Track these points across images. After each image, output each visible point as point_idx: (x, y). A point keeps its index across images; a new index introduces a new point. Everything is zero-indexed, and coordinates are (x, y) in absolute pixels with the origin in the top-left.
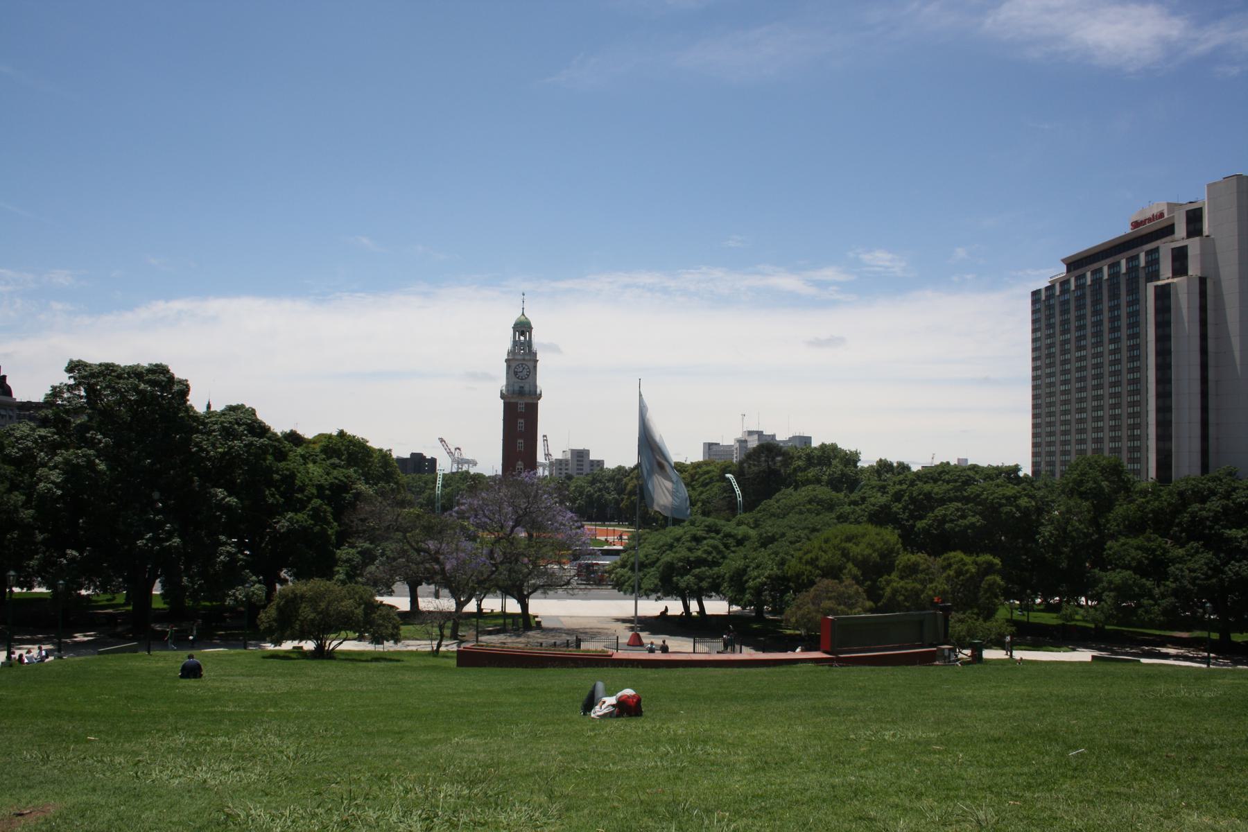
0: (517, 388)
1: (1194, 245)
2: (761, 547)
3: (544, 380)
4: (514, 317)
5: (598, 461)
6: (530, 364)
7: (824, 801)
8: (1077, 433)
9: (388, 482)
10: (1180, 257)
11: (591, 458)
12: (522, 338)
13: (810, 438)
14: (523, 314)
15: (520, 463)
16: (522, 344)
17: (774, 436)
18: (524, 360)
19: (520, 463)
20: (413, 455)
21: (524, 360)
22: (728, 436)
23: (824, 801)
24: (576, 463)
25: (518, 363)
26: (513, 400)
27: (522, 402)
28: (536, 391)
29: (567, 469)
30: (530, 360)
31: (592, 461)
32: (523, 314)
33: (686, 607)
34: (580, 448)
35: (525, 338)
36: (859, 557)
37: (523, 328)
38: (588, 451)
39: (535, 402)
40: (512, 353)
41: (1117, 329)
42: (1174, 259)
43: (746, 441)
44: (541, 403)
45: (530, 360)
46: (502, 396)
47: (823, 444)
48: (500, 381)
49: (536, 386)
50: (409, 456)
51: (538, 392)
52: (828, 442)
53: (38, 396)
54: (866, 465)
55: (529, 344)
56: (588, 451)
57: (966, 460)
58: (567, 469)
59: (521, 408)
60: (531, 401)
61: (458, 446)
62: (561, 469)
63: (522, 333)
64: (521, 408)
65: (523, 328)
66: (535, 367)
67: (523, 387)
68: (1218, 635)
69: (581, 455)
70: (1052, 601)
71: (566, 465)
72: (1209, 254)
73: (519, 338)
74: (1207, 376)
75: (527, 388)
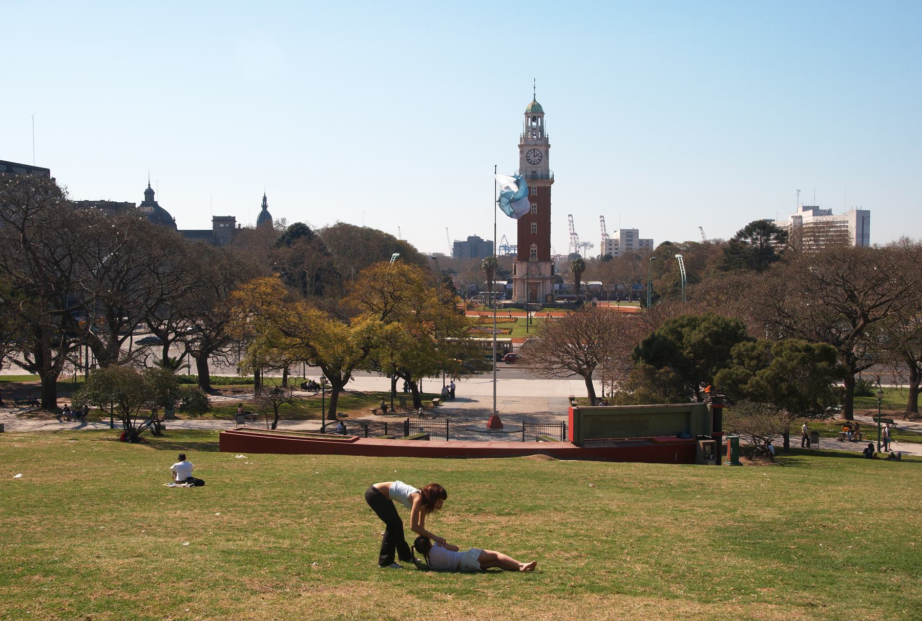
0: (529, 173)
3: (556, 164)
4: (527, 105)
5: (647, 241)
6: (542, 149)
7: (158, 274)
11: (640, 238)
12: (534, 124)
13: (869, 211)
14: (535, 101)
15: (534, 245)
16: (535, 129)
19: (534, 245)
20: (469, 238)
21: (536, 145)
23: (158, 274)
24: (625, 242)
25: (531, 148)
28: (548, 175)
29: (617, 249)
30: (542, 145)
31: (641, 241)
32: (535, 101)
34: (630, 227)
35: (538, 124)
36: (732, 324)
37: (535, 113)
38: (638, 230)
40: (524, 138)
43: (801, 217)
44: (554, 188)
49: (548, 170)
50: (466, 240)
55: (541, 129)
56: (638, 230)
58: (617, 249)
61: (570, 214)
62: (610, 249)
63: (534, 119)
65: (535, 113)
66: (547, 152)
69: (629, 235)
71: (616, 245)
73: (531, 124)
75: (539, 173)
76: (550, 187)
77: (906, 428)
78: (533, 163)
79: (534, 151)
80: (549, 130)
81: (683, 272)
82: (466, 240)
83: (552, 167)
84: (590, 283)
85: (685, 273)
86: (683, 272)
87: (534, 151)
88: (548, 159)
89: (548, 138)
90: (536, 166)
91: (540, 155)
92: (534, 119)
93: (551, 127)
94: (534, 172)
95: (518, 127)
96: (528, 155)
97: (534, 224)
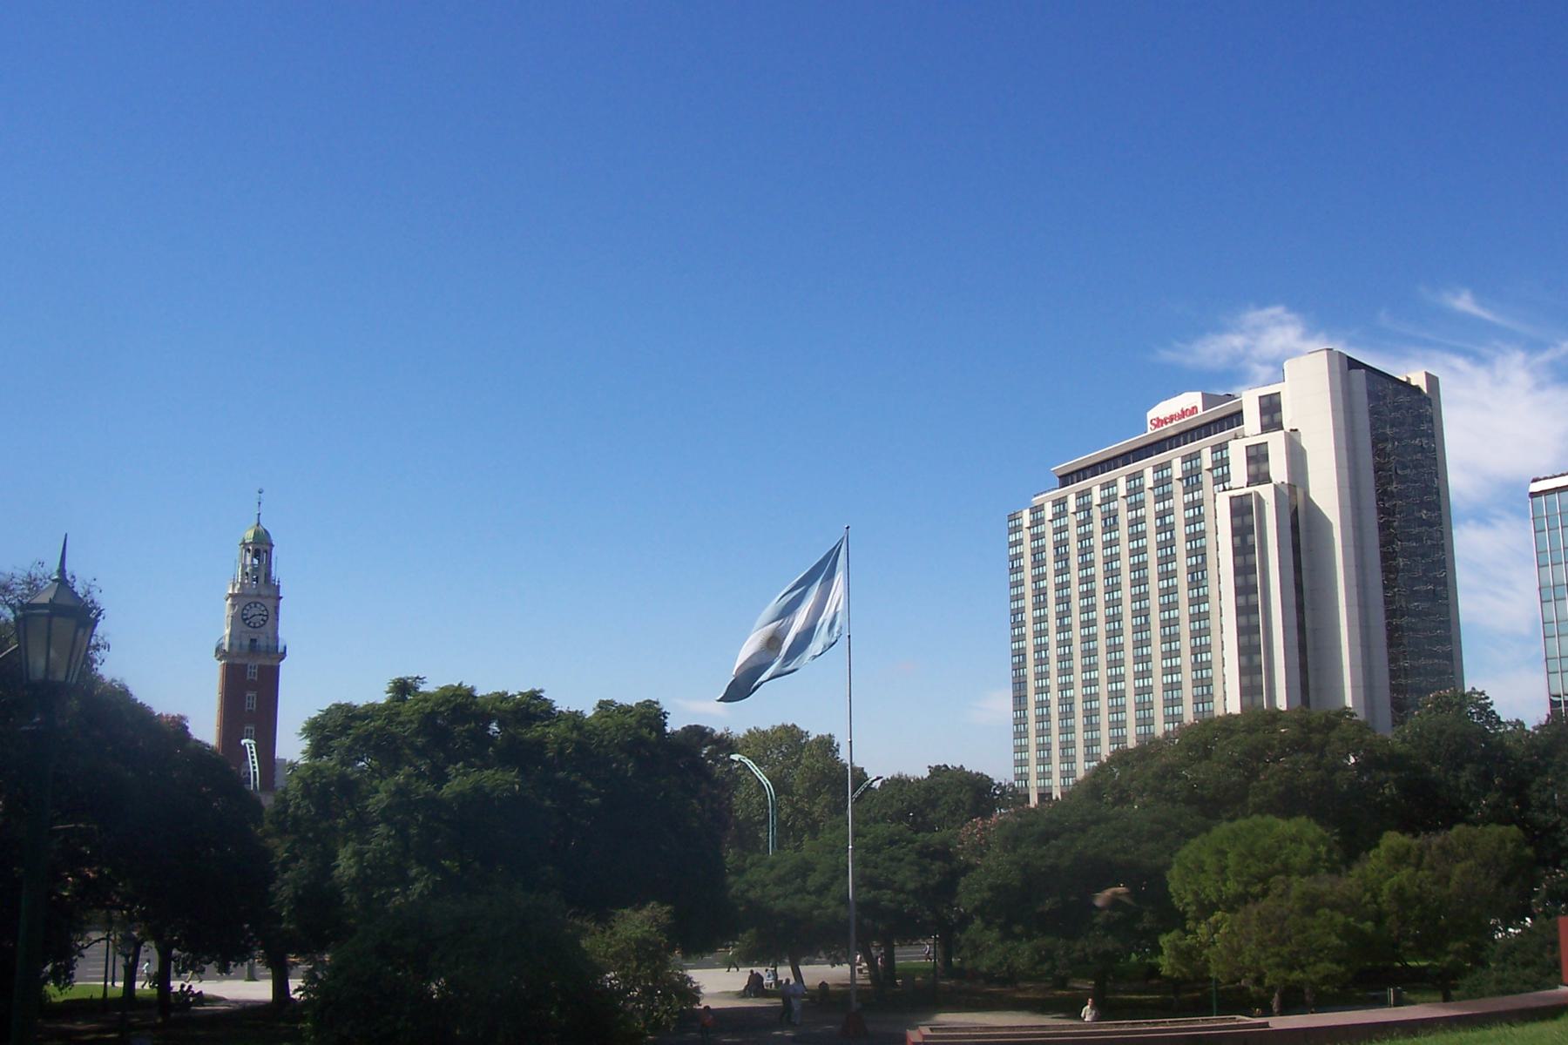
1: (1276, 444)
2: (1417, 871)
3: (290, 629)
6: (269, 604)
8: (1123, 691)
10: (1257, 456)
17: (472, 689)
18: (259, 595)
22: (779, 724)
25: (249, 600)
26: (238, 661)
27: (254, 664)
28: (277, 647)
30: (269, 596)
32: (258, 524)
33: (280, 988)
37: (261, 547)
39: (274, 663)
42: (1250, 459)
44: (284, 666)
45: (269, 596)
46: (220, 652)
47: (535, 695)
48: (221, 627)
49: (276, 639)
51: (281, 649)
52: (693, 724)
53: (928, 774)
54: (678, 728)
57: (507, 693)
59: (252, 675)
60: (267, 662)
64: (252, 675)
65: (261, 547)
66: (277, 608)
67: (255, 640)
68: (780, 1001)
72: (1296, 456)
73: (252, 561)
75: (262, 642)
76: (279, 666)
78: (253, 605)
79: (247, 619)
80: (278, 572)
81: (254, 768)
82: (926, 774)
83: (284, 634)
85: (257, 770)
86: (254, 768)
87: (247, 619)
88: (278, 620)
89: (278, 586)
90: (257, 630)
91: (265, 618)
92: (257, 554)
93: (282, 569)
94: (253, 641)
95: (229, 573)
96: (245, 612)
97: (249, 728)
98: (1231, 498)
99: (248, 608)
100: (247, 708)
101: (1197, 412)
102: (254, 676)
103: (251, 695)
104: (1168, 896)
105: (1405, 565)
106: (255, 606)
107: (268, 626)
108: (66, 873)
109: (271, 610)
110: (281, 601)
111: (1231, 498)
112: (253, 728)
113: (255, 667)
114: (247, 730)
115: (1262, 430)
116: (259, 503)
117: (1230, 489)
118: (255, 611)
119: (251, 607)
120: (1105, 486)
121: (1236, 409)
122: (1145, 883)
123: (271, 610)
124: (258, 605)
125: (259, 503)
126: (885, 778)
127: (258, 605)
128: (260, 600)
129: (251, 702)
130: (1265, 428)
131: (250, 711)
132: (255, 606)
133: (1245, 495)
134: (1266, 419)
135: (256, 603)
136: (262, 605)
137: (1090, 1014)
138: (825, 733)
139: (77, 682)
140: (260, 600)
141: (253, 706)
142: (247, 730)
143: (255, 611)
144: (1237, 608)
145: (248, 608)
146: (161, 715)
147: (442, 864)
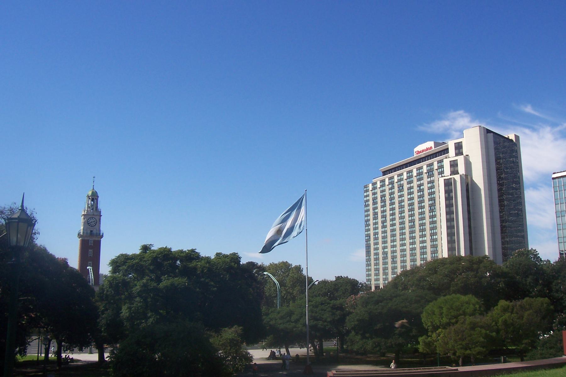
3: (105, 227)
5: (562, 348)
6: (97, 218)
9: (356, 293)
10: (454, 165)
17: (171, 249)
18: (93, 215)
22: (281, 261)
25: (90, 217)
26: (86, 238)
27: (92, 239)
28: (100, 233)
30: (97, 215)
32: (93, 189)
37: (94, 197)
39: (99, 239)
41: (410, 205)
42: (451, 166)
44: (103, 240)
45: (97, 215)
46: (79, 235)
47: (193, 251)
48: (80, 226)
49: (100, 230)
51: (101, 234)
52: (250, 261)
53: (335, 279)
54: (245, 263)
57: (183, 250)
59: (91, 243)
60: (97, 239)
64: (91, 243)
65: (94, 197)
66: (100, 219)
67: (92, 231)
70: (160, 311)
72: (468, 165)
73: (91, 202)
74: (469, 235)
75: (95, 232)
76: (101, 240)
77: (281, 226)
78: (91, 218)
79: (89, 223)
80: (100, 206)
81: (92, 277)
83: (102, 229)
84: (26, 298)
85: (93, 278)
86: (92, 277)
88: (100, 224)
89: (101, 212)
90: (93, 227)
91: (96, 223)
92: (93, 200)
93: (102, 205)
94: (92, 231)
95: (83, 207)
96: (89, 221)
97: (90, 263)
98: (444, 180)
99: (89, 219)
100: (89, 256)
101: (432, 149)
102: (92, 244)
103: (91, 251)
104: (422, 323)
105: (507, 204)
106: (92, 219)
107: (97, 226)
108: (24, 315)
109: (98, 220)
110: (102, 217)
111: (444, 180)
112: (91, 263)
113: (92, 241)
114: (89, 263)
115: (456, 155)
116: (94, 182)
117: (444, 176)
118: (92, 220)
119: (91, 219)
120: (399, 175)
121: (446, 148)
122: (413, 318)
123: (98, 220)
124: (93, 218)
125: (94, 182)
126: (319, 281)
127: (93, 218)
128: (94, 216)
129: (91, 253)
130: (457, 155)
131: (90, 257)
132: (92, 219)
133: (450, 179)
134: (457, 151)
135: (92, 218)
136: (95, 218)
137: (394, 366)
138: (298, 265)
139: (28, 246)
140: (94, 216)
141: (91, 255)
142: (89, 263)
143: (92, 220)
144: (447, 219)
145: (89, 219)
146: (58, 258)
147: (160, 312)
